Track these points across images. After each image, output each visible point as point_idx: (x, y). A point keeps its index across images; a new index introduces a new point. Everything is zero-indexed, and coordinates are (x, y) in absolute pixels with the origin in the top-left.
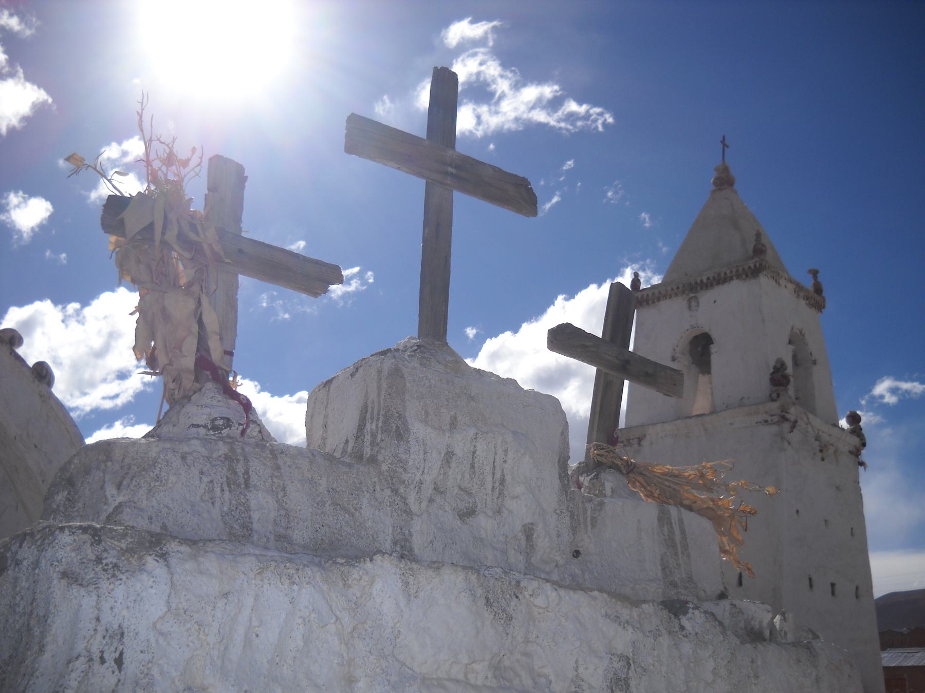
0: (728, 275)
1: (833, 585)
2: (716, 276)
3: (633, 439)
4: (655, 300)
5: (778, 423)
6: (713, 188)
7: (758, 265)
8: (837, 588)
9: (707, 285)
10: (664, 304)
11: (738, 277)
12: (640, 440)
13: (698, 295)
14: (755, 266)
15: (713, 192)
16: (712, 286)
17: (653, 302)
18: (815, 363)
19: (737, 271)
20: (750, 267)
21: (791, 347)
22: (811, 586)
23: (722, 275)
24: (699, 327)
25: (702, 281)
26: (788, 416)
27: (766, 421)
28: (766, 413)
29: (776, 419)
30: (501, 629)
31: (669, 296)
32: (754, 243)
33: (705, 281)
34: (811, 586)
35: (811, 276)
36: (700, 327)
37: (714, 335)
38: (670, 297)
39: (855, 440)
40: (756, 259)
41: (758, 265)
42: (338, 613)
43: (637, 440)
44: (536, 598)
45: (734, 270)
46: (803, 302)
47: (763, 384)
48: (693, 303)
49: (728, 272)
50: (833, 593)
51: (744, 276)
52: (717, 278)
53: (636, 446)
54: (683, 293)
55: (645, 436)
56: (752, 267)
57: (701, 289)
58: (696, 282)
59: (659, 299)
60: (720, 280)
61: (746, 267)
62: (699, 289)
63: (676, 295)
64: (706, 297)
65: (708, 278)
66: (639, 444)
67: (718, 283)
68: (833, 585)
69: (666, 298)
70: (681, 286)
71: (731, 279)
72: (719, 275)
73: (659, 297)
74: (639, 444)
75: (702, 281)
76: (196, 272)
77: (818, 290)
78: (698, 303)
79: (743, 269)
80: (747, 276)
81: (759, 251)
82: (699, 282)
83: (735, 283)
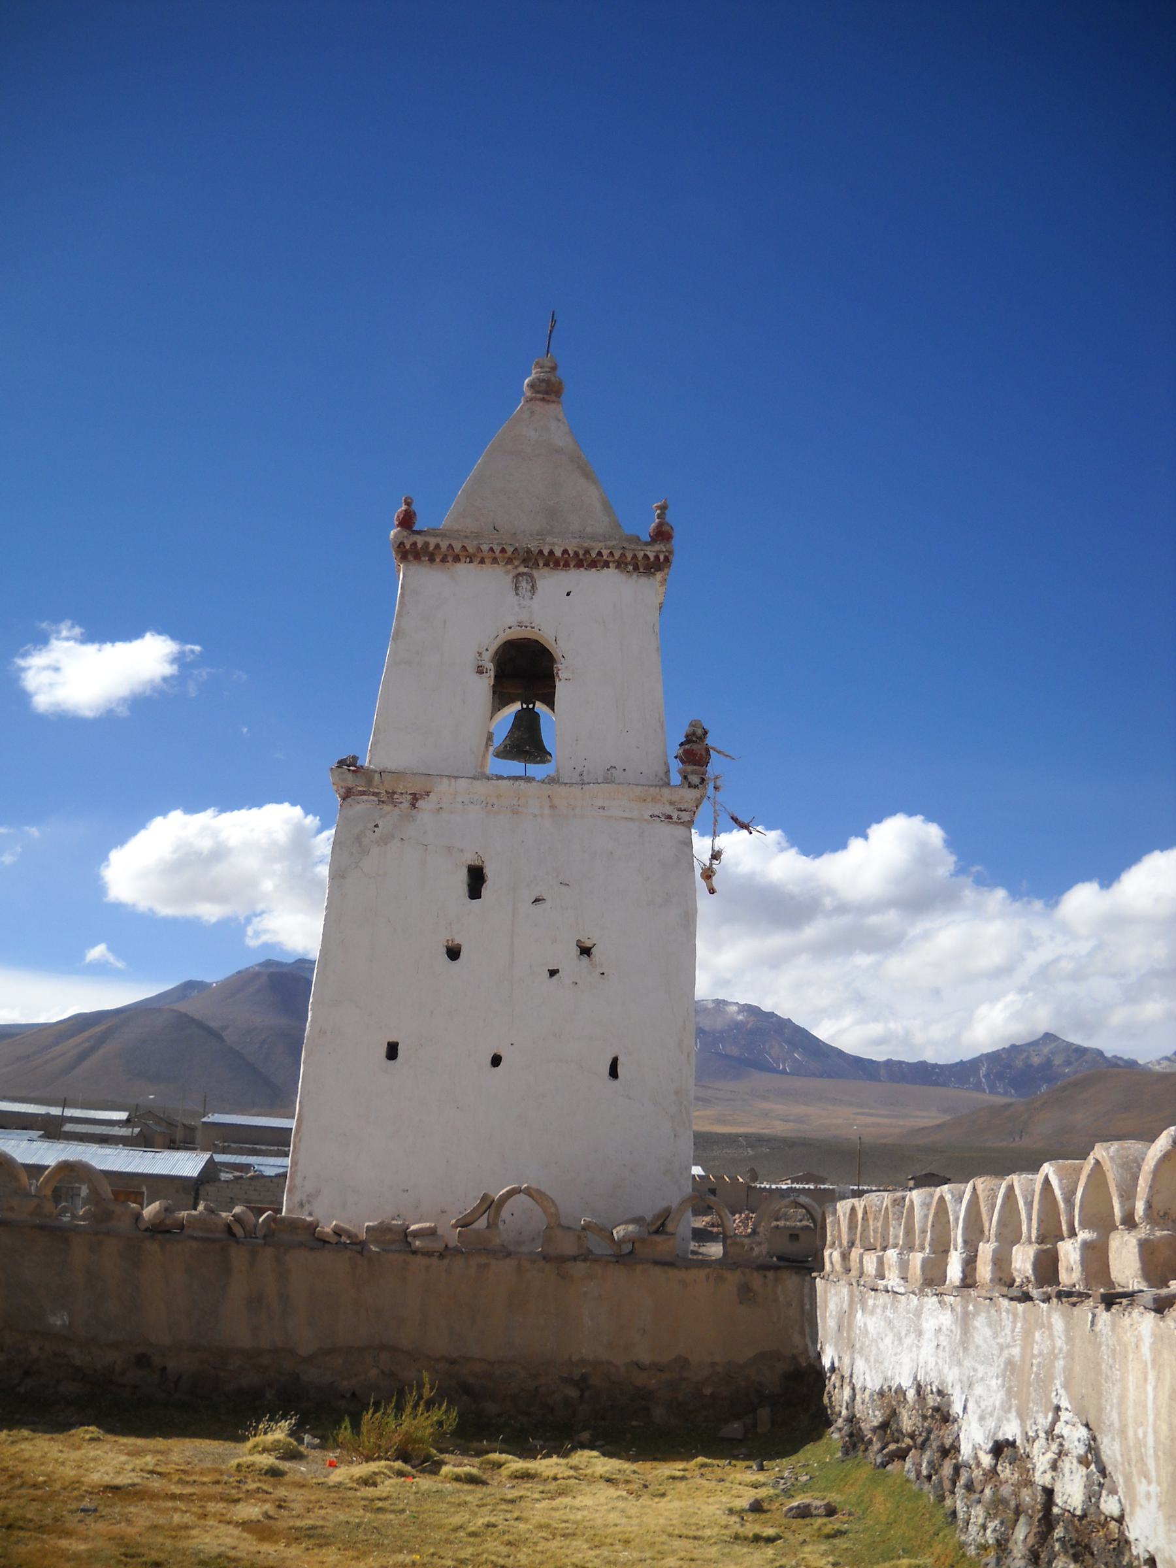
0: (605, 557)
2: (581, 552)
3: (402, 794)
4: (450, 559)
7: (662, 557)
9: (555, 562)
10: (463, 570)
11: (621, 564)
12: (415, 798)
13: (535, 573)
14: (657, 557)
16: (567, 565)
19: (623, 555)
20: (646, 557)
23: (594, 555)
24: (533, 628)
25: (551, 553)
27: (670, 817)
28: (672, 803)
31: (479, 559)
33: (558, 553)
36: (536, 630)
38: (482, 561)
40: (658, 547)
41: (662, 557)
43: (409, 797)
45: (617, 554)
49: (605, 552)
51: (630, 568)
52: (581, 557)
53: (406, 805)
54: (509, 561)
55: (428, 794)
56: (652, 556)
57: (546, 564)
58: (541, 552)
59: (457, 559)
60: (586, 560)
61: (640, 555)
62: (541, 565)
63: (495, 561)
64: (551, 582)
65: (565, 552)
66: (413, 805)
67: (580, 564)
69: (471, 562)
70: (510, 550)
71: (606, 565)
72: (587, 552)
73: (458, 555)
74: (413, 805)
75: (551, 553)
76: (549, 401)
78: (533, 588)
79: (635, 557)
80: (636, 568)
82: (546, 552)
83: (611, 573)
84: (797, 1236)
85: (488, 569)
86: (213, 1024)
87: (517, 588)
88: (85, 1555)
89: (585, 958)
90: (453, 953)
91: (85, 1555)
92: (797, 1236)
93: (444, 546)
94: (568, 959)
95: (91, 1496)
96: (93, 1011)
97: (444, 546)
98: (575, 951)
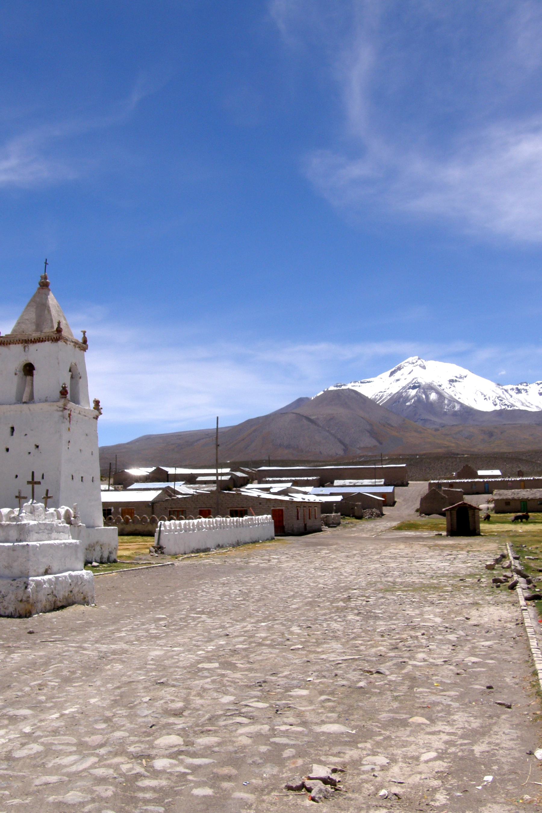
1: (82, 477)
5: (62, 411)
6: (39, 286)
8: (84, 478)
10: (12, 346)
15: (39, 289)
16: (36, 342)
17: (7, 344)
18: (80, 378)
21: (70, 373)
22: (73, 479)
26: (66, 408)
29: (61, 409)
30: (377, 784)
32: (57, 326)
34: (73, 479)
35: (82, 333)
37: (36, 366)
38: (16, 344)
39: (96, 412)
42: (357, 662)
44: (248, 799)
46: (77, 349)
47: (57, 394)
48: (27, 349)
50: (82, 481)
54: (22, 343)
59: (10, 344)
63: (18, 343)
64: (33, 347)
67: (39, 342)
68: (82, 477)
71: (45, 341)
77: (85, 341)
81: (59, 330)
83: (47, 343)
84: (509, 502)
85: (17, 345)
86: (313, 418)
87: (25, 350)
88: (191, 752)
89: (37, 449)
90: (7, 450)
91: (191, 752)
92: (509, 502)
93: (6, 341)
94: (32, 449)
95: (52, 668)
96: (168, 432)
97: (6, 341)
98: (34, 447)
